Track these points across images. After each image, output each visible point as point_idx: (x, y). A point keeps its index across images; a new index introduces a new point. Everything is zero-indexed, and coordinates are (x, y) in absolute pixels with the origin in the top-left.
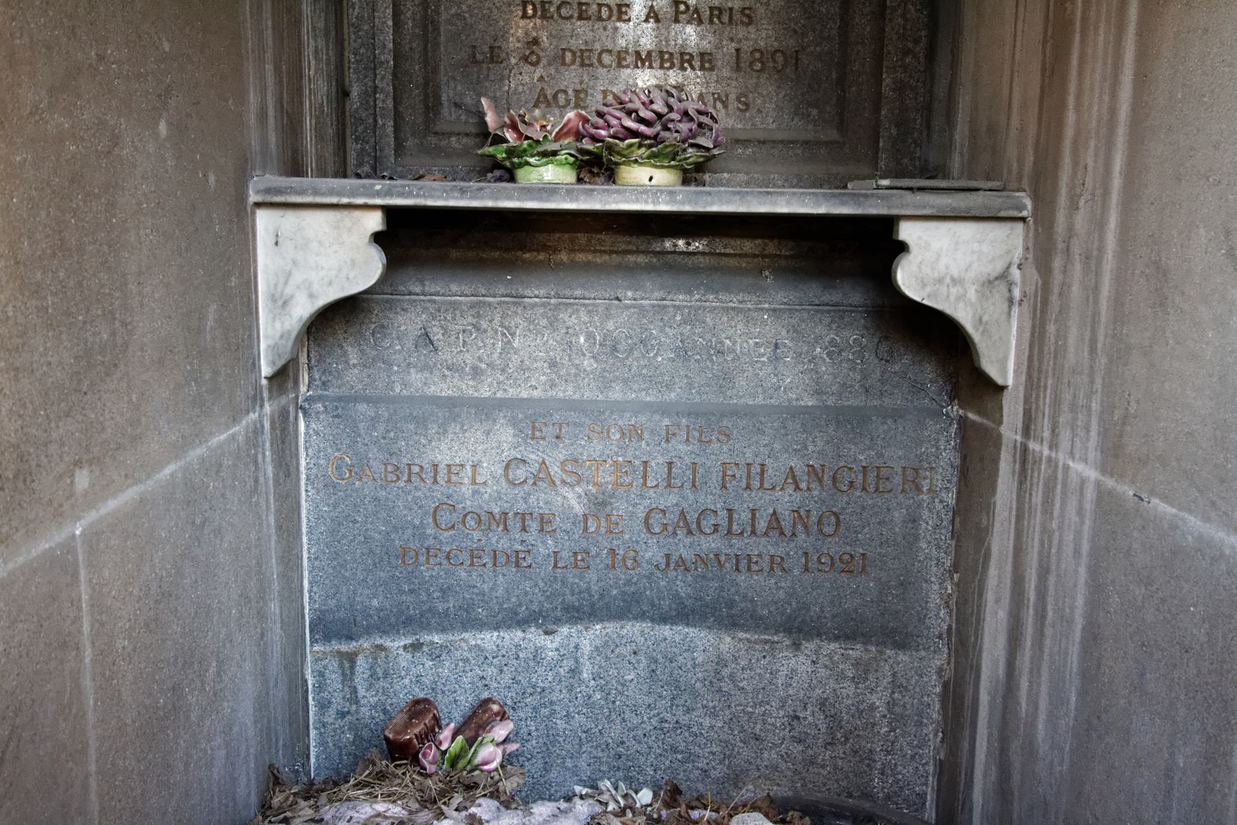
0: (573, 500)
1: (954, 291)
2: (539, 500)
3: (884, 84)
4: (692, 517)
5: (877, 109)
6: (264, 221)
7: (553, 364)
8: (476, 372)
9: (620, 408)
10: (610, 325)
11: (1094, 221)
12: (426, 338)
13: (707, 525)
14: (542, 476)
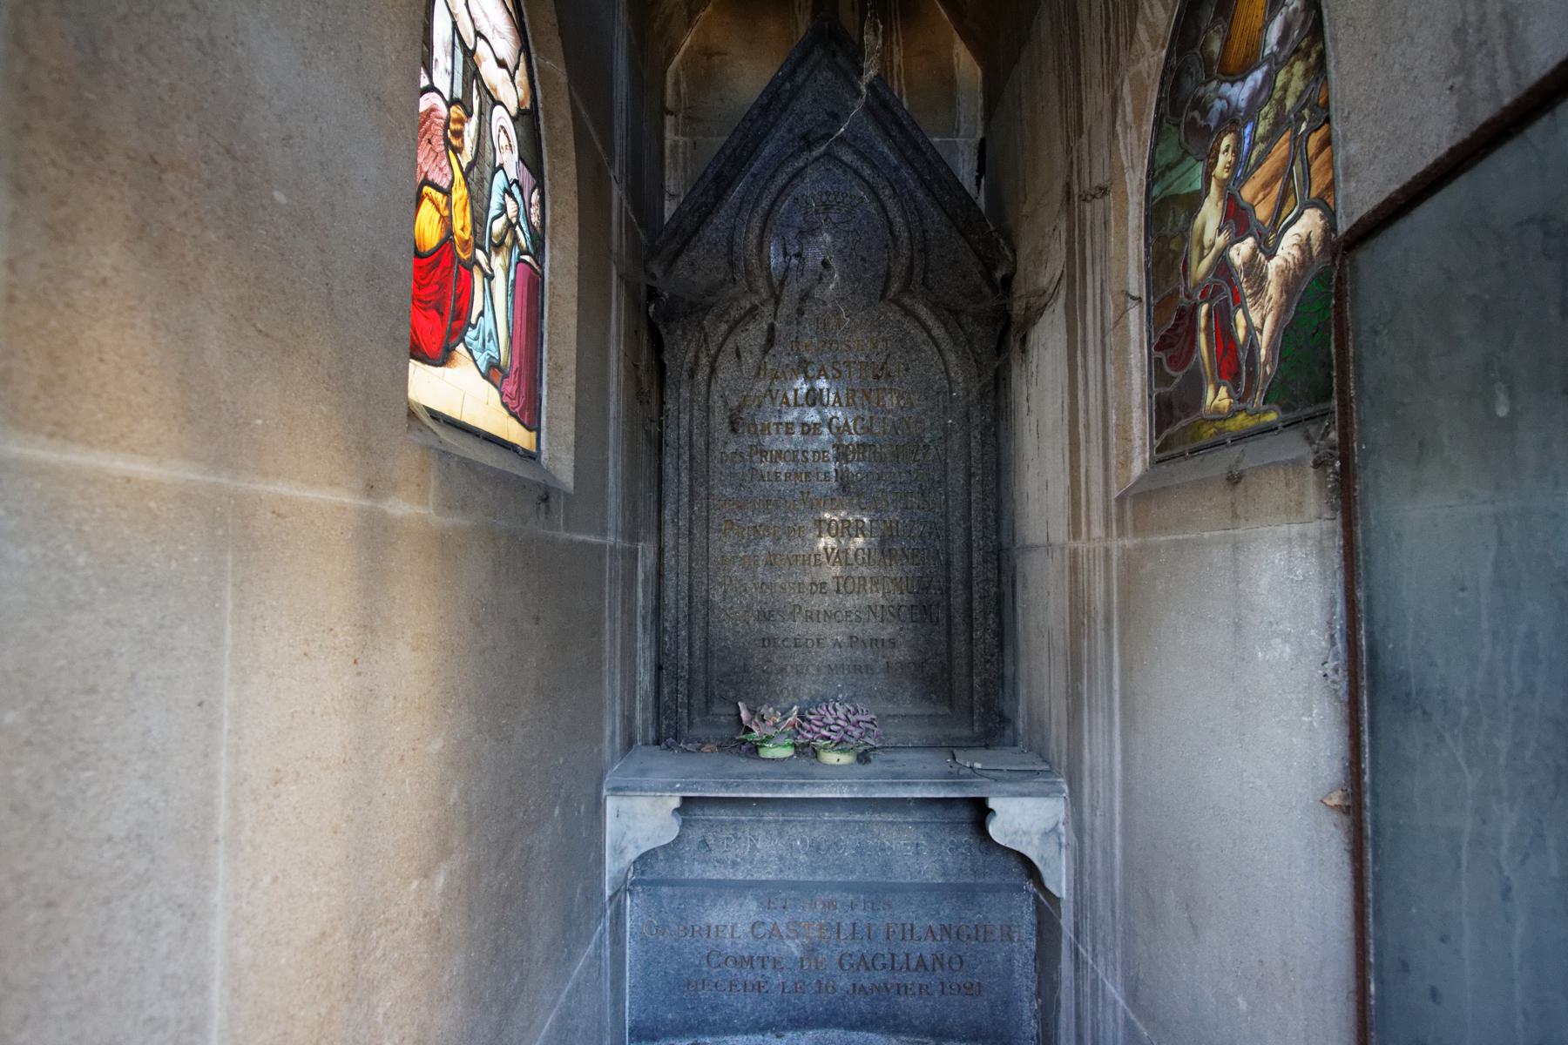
0: (794, 948)
1: (1025, 839)
2: (772, 949)
4: (869, 959)
5: (971, 697)
6: (611, 804)
7: (781, 858)
8: (734, 864)
9: (822, 886)
10: (816, 834)
11: (1102, 750)
12: (704, 843)
13: (878, 964)
14: (774, 933)
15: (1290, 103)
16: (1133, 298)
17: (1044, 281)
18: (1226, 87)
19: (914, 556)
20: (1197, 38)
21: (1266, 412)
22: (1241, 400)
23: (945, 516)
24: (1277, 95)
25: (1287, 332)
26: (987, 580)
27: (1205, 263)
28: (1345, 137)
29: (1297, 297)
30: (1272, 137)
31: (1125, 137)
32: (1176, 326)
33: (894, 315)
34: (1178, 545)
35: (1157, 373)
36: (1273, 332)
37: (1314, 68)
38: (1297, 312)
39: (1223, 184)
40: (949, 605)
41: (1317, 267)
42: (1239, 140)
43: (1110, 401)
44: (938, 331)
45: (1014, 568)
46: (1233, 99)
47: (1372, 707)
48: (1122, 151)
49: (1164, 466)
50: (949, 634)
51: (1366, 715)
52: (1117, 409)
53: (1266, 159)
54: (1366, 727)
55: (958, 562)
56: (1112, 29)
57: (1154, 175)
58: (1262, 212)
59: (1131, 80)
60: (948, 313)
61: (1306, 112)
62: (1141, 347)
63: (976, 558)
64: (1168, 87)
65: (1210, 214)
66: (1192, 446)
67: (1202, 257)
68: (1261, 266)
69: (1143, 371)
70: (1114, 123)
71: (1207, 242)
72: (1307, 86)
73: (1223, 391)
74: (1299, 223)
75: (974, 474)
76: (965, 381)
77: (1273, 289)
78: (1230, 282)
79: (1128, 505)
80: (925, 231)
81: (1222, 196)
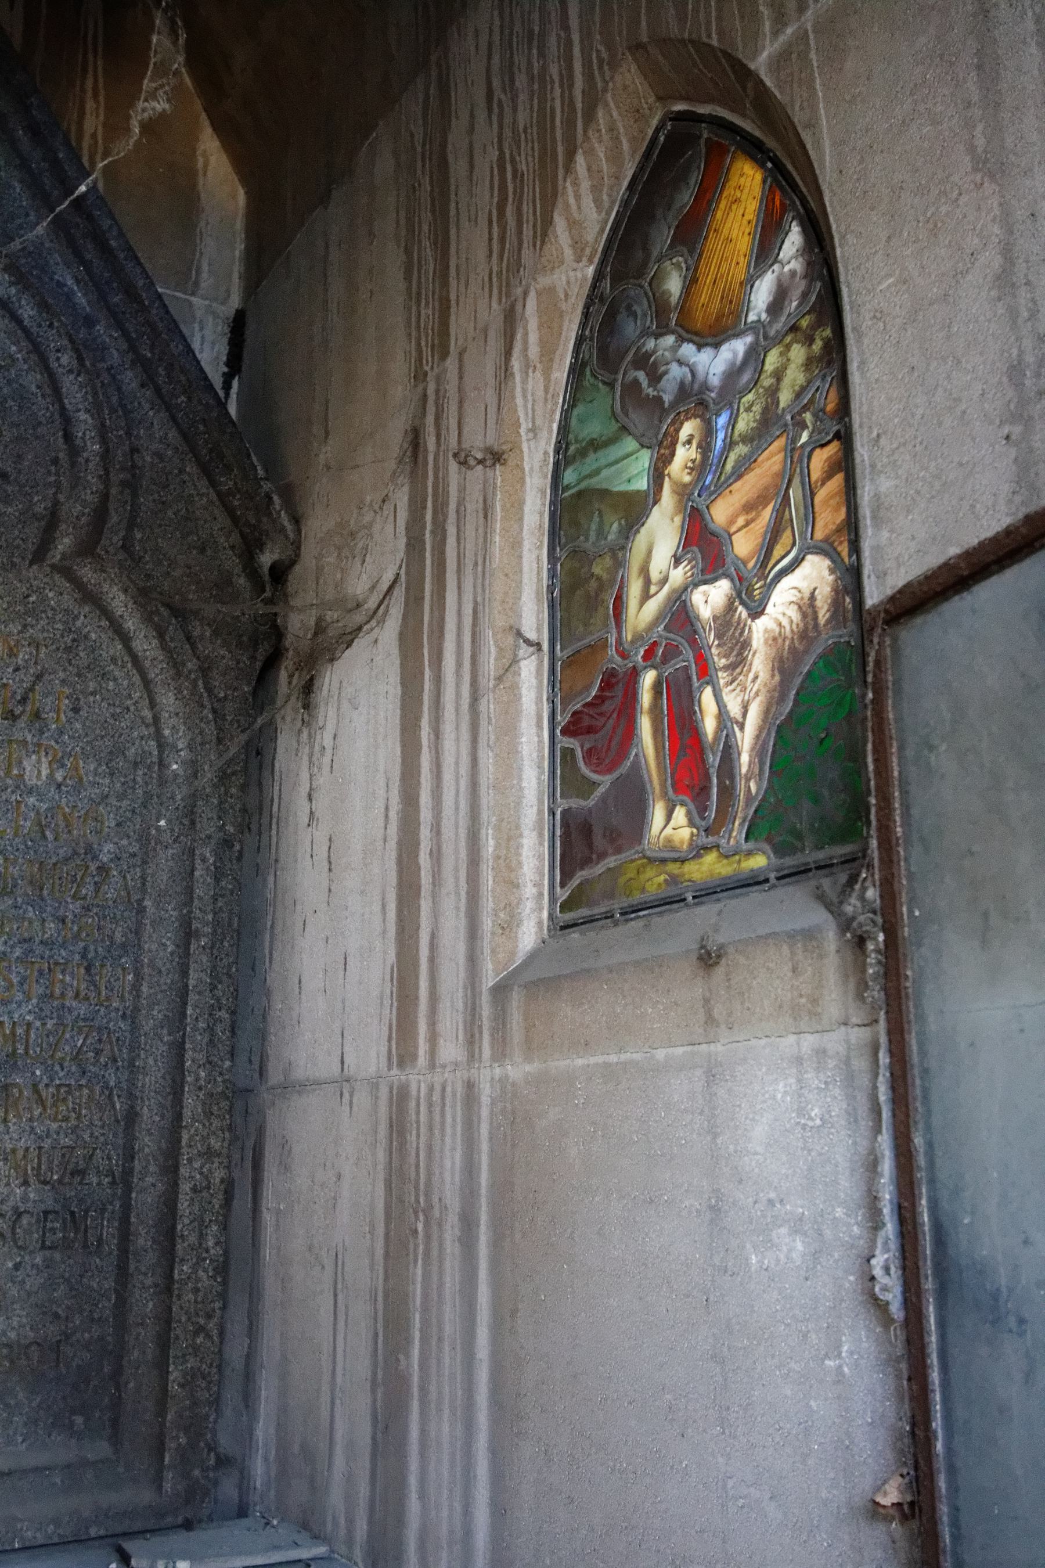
3: (171, 1378)
5: (161, 1408)
15: (785, 397)
16: (528, 642)
17: (358, 585)
18: (688, 350)
19: (57, 1100)
20: (645, 264)
21: (749, 854)
22: (710, 831)
23: (132, 1017)
24: (767, 382)
25: (784, 734)
26: (209, 1154)
27: (652, 607)
28: (873, 466)
29: (798, 681)
30: (759, 437)
31: (525, 381)
32: (600, 699)
33: (59, 596)
34: (609, 1072)
35: (565, 775)
36: (760, 729)
37: (820, 359)
38: (796, 701)
39: (683, 492)
40: (127, 1208)
41: (826, 640)
42: (708, 432)
43: (484, 816)
44: (145, 644)
45: (261, 1131)
46: (701, 370)
47: (942, 1324)
48: (519, 401)
49: (575, 935)
50: (123, 1274)
51: (934, 1339)
52: (498, 828)
53: (748, 469)
54: (934, 1359)
55: (150, 1115)
56: (510, 210)
57: (567, 451)
58: (744, 545)
59: (539, 294)
60: (168, 612)
61: (808, 417)
62: (539, 726)
63: (190, 1102)
64: (596, 322)
65: (661, 534)
66: (625, 902)
67: (646, 596)
68: (741, 626)
69: (540, 767)
70: (508, 353)
71: (655, 575)
72: (809, 382)
73: (680, 815)
74: (798, 572)
75: (197, 934)
76: (190, 748)
77: (760, 663)
78: (693, 642)
79: (516, 999)
80: (134, 450)
81: (680, 507)
